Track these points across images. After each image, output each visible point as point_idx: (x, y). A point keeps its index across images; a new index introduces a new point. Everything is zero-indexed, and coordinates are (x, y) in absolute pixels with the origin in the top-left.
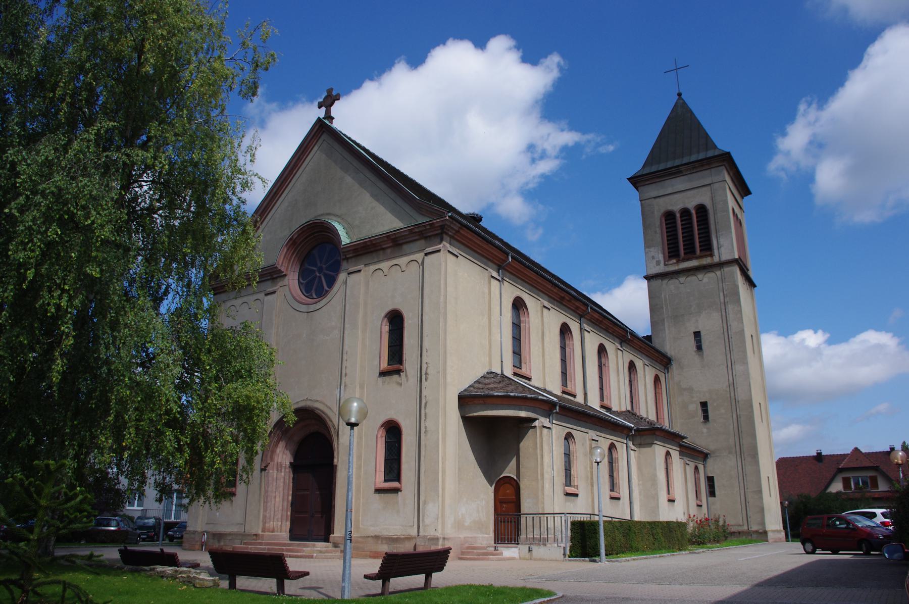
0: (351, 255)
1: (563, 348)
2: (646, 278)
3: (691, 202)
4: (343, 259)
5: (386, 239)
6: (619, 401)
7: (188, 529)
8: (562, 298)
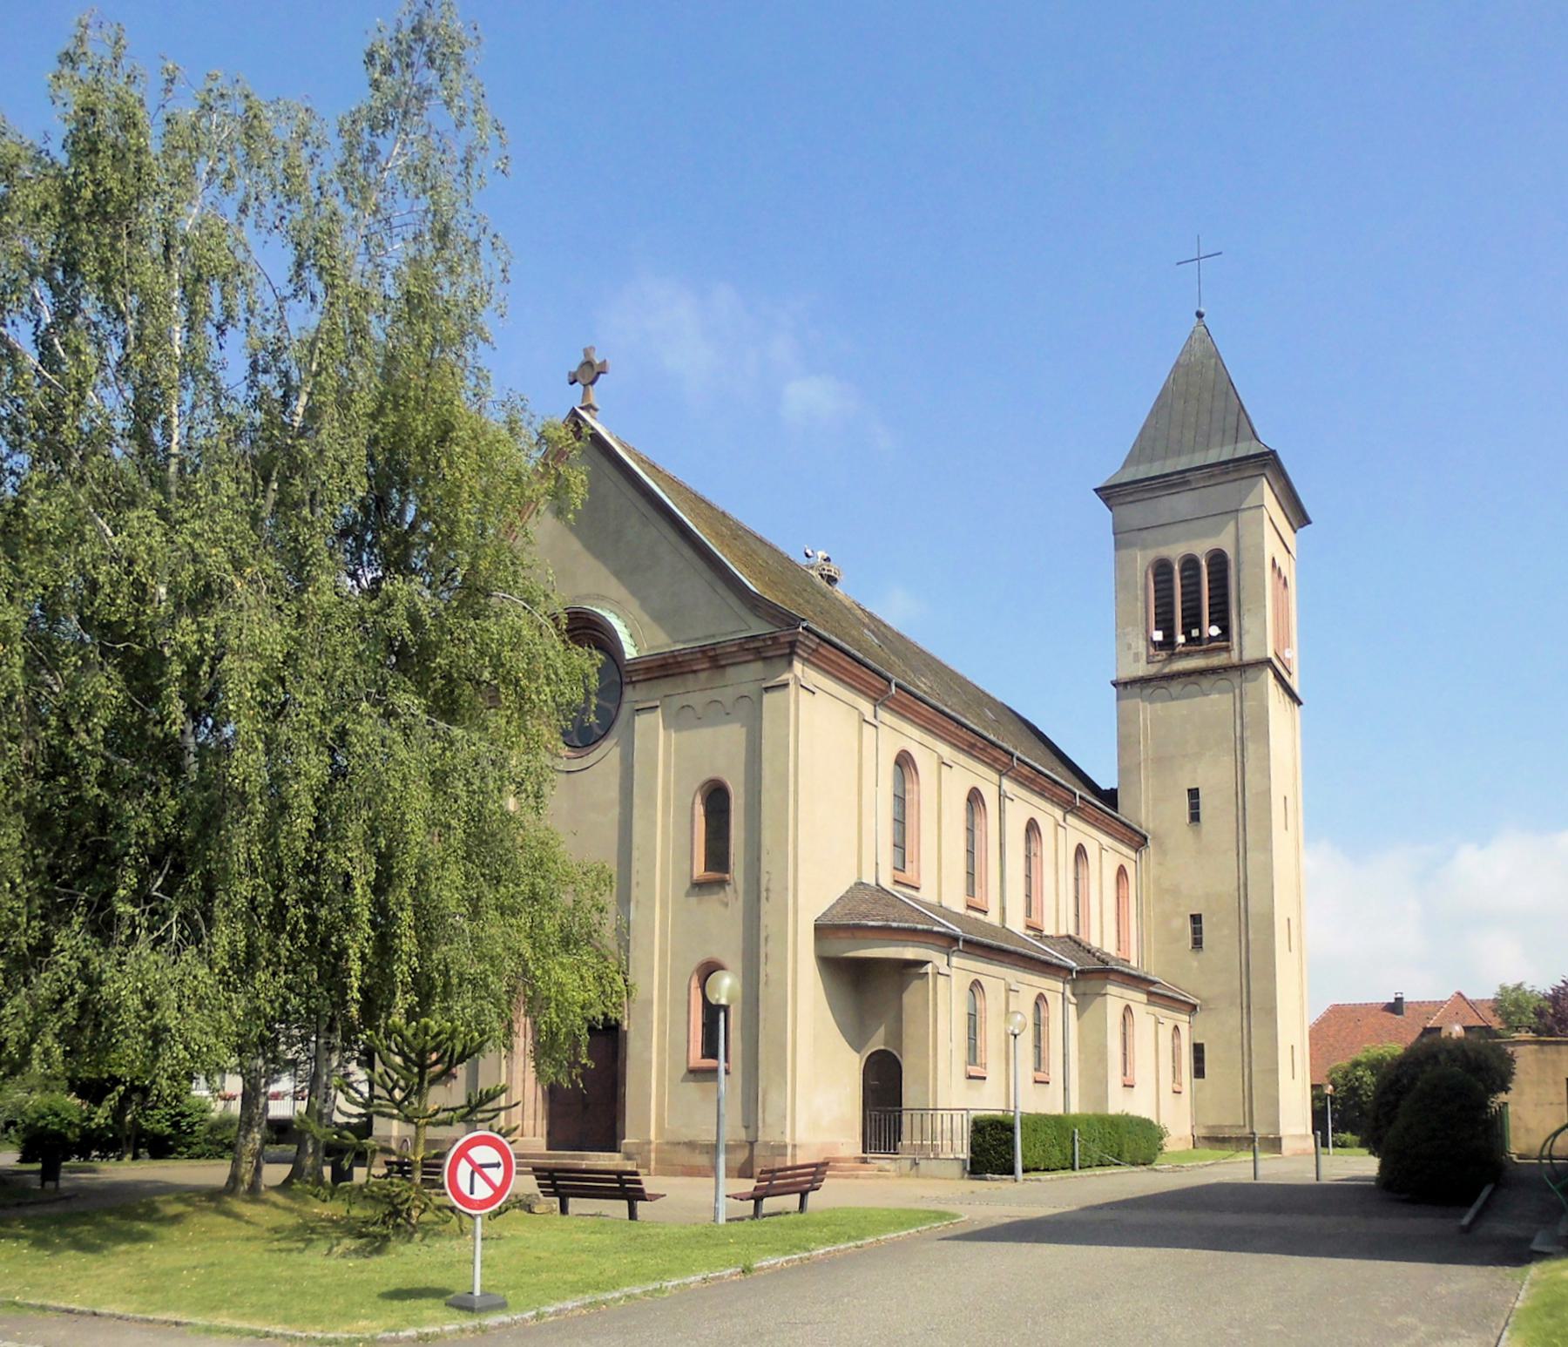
0: (640, 678)
1: (970, 830)
2: (1115, 684)
3: (1200, 549)
4: (627, 683)
5: (699, 655)
6: (1058, 922)
7: (1166, 1149)
8: (972, 746)
